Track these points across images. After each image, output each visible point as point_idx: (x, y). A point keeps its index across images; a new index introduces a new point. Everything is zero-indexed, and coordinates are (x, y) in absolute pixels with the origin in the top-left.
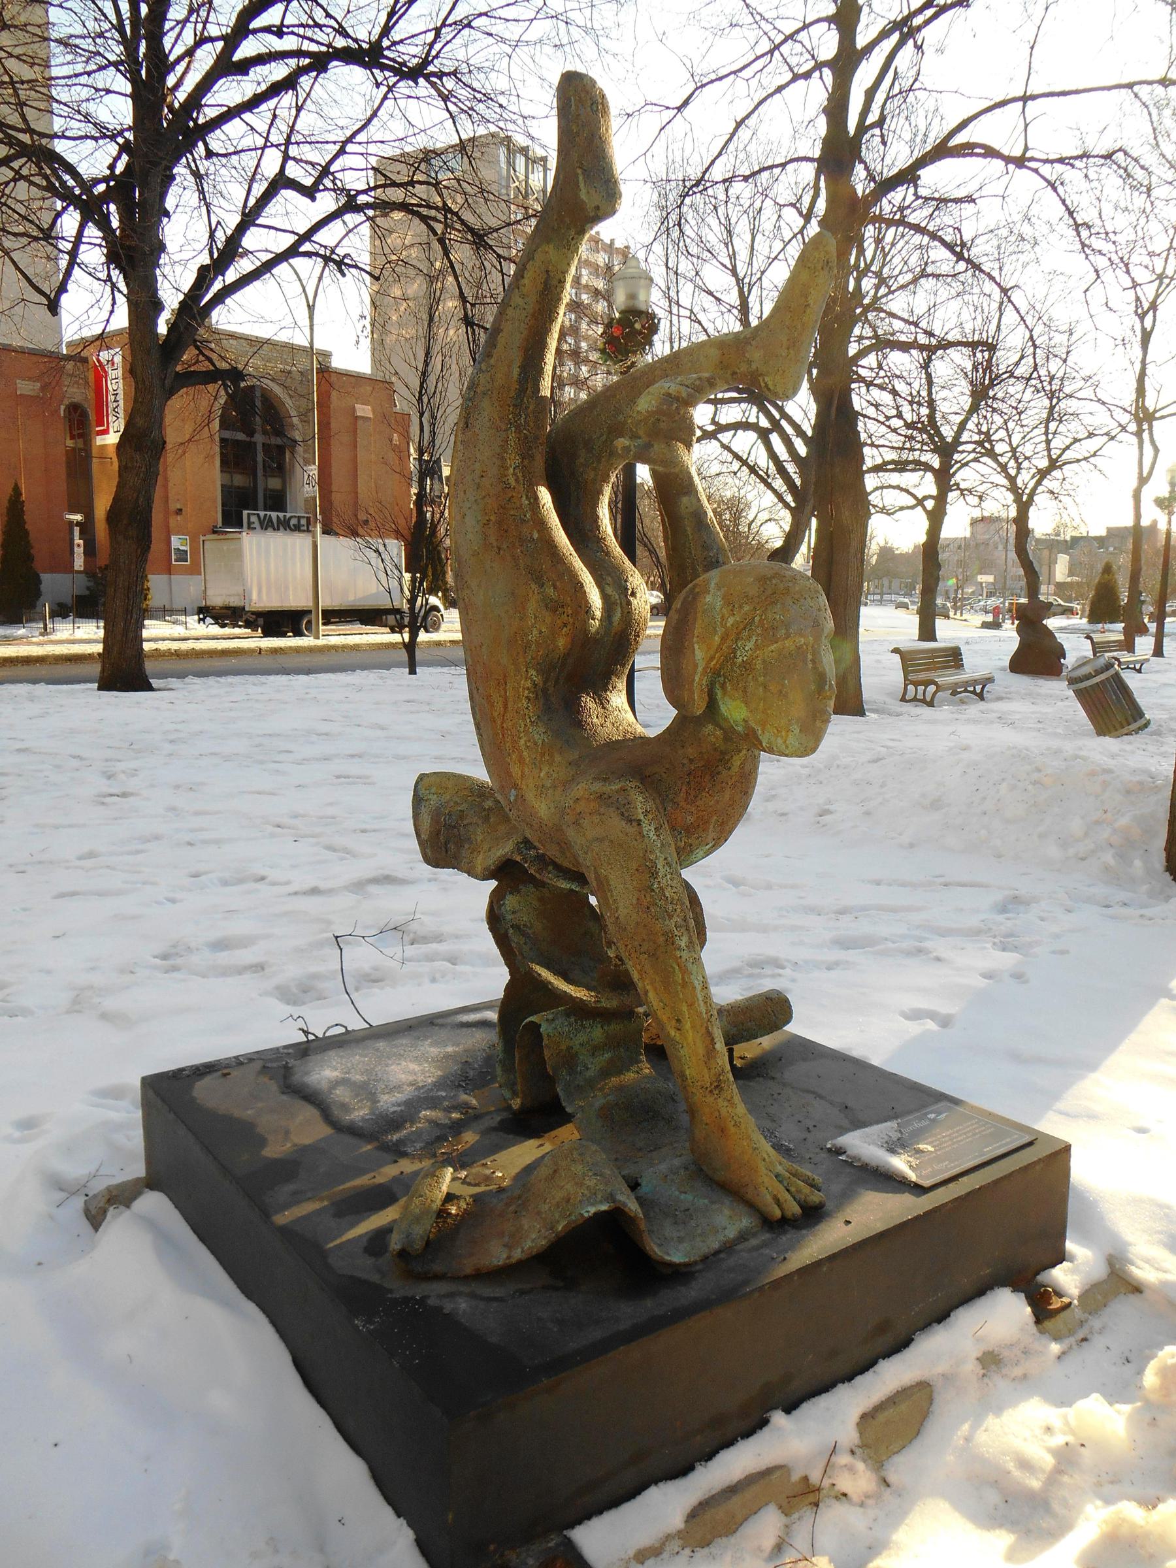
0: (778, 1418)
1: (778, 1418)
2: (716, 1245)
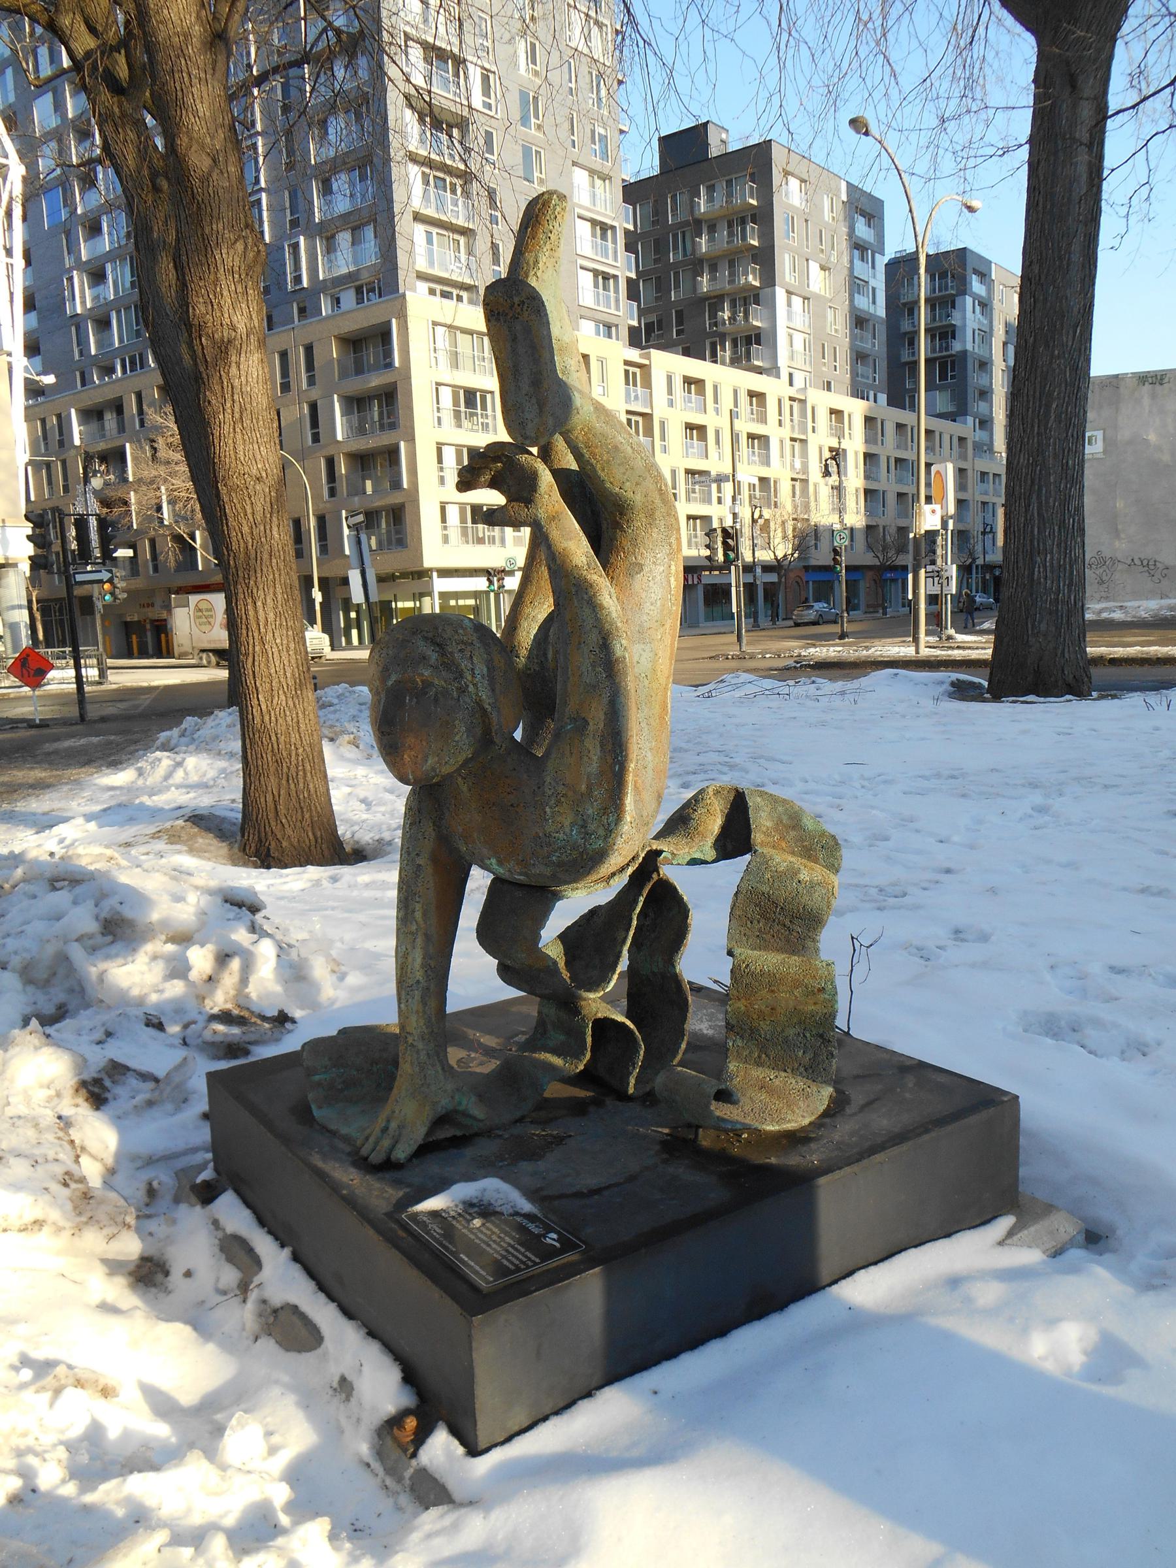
0: (286, 1252)
1: (286, 1252)
2: (333, 1127)
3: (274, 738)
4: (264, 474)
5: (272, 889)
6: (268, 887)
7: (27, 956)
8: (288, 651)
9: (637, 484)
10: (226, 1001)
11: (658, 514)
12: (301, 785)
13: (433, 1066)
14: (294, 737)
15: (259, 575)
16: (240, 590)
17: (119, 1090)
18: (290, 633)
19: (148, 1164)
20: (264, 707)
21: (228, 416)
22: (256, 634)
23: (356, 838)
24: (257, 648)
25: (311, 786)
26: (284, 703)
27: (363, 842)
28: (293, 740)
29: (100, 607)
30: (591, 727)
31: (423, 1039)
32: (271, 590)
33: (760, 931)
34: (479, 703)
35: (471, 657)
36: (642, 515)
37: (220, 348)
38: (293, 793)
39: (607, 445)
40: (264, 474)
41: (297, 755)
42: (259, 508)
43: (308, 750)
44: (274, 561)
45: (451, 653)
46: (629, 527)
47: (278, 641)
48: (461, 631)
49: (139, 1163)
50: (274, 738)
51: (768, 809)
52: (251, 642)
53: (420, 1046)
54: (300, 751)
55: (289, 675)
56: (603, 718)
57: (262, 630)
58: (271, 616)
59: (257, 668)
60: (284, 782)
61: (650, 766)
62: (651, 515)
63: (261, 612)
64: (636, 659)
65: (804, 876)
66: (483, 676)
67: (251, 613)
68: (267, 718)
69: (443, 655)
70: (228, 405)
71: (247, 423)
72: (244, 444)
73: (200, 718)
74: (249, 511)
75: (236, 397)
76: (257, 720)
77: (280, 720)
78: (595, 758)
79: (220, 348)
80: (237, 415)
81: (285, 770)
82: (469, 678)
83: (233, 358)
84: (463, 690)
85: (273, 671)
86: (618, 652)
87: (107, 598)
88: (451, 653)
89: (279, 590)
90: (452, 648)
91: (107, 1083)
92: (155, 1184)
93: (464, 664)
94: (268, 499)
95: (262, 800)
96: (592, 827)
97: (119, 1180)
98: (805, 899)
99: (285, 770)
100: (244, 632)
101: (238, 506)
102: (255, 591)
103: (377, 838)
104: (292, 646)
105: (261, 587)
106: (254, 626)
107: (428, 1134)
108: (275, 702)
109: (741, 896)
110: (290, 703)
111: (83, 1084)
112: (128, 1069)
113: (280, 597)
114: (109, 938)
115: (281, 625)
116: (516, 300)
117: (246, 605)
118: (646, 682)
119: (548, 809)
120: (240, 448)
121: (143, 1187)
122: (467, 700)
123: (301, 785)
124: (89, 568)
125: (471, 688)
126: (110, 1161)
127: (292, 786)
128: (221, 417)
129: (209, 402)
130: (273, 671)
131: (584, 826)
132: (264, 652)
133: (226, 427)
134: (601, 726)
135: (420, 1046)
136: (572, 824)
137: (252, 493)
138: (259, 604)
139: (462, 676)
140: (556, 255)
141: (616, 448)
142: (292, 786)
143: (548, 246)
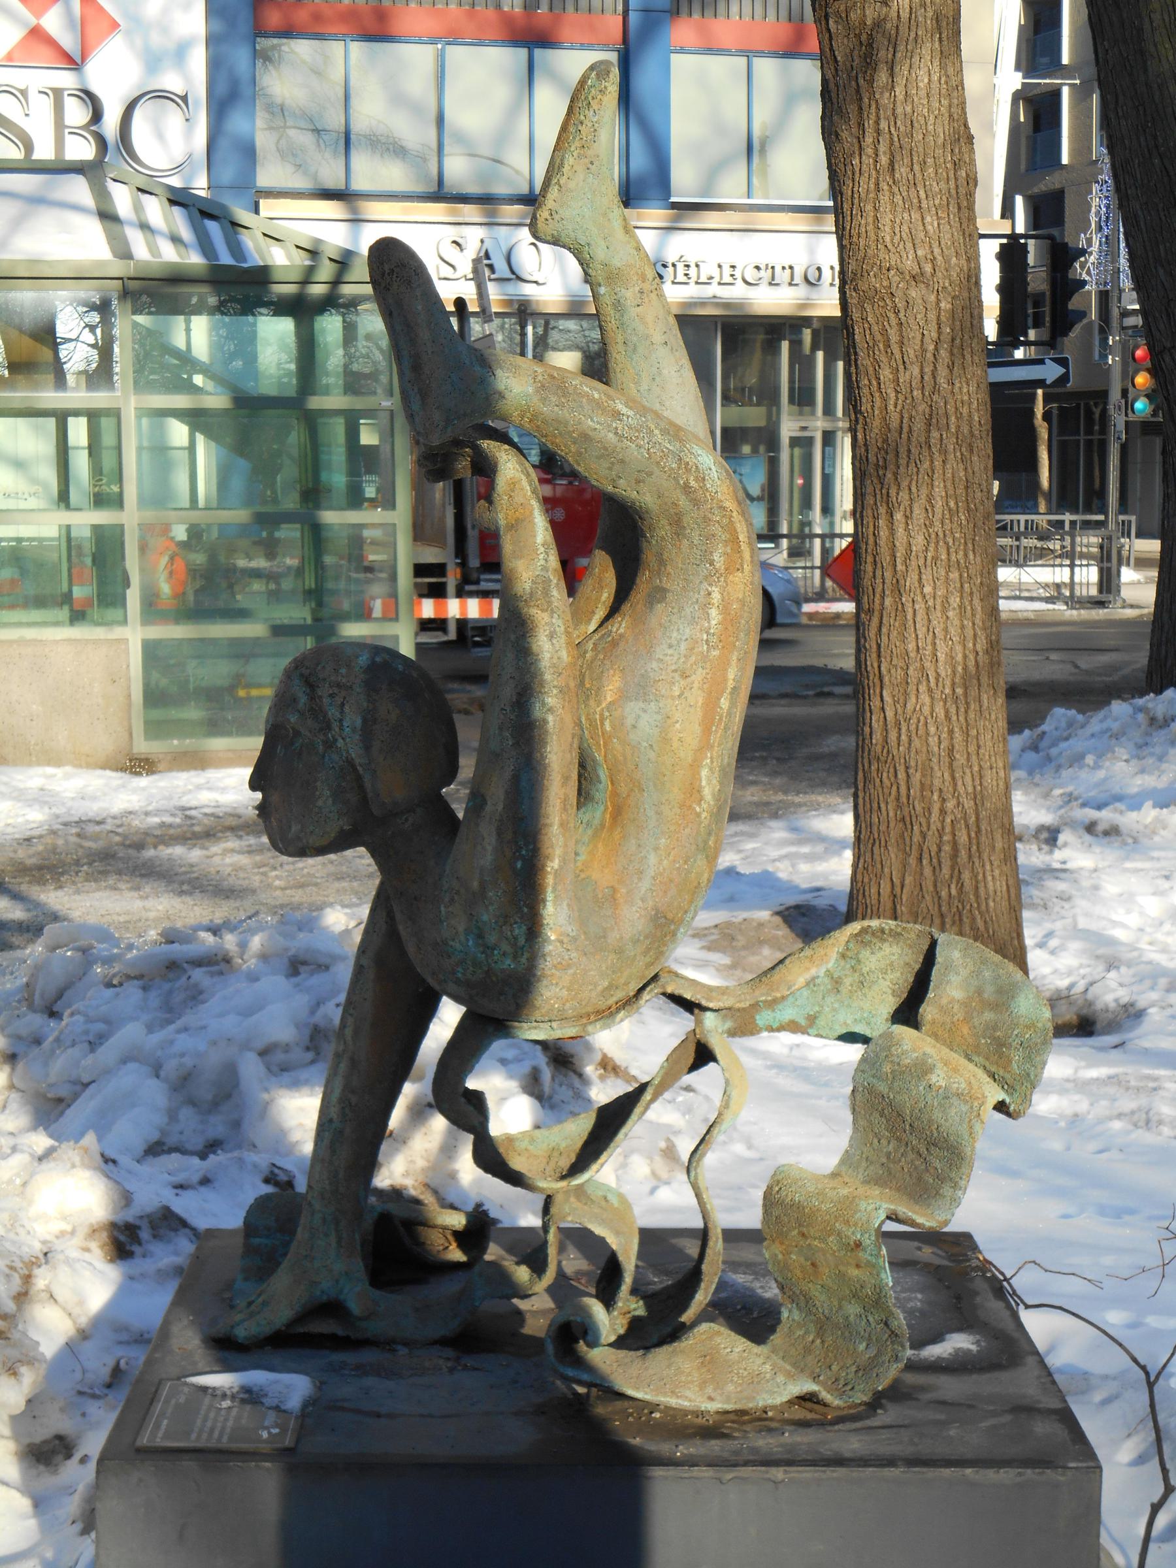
3: (901, 775)
4: (928, 268)
5: (795, 1052)
6: (791, 1049)
7: (188, 1062)
8: (944, 610)
9: (638, 482)
10: (406, 1174)
11: (686, 520)
12: (946, 871)
13: (326, 1235)
14: (940, 776)
15: (903, 462)
16: (870, 489)
17: (157, 1248)
18: (954, 575)
19: (136, 1341)
20: (890, 714)
21: (868, 161)
22: (888, 575)
23: (1090, 996)
24: (888, 601)
25: (966, 876)
26: (926, 710)
27: (1099, 1006)
28: (937, 783)
29: (1121, 426)
30: (489, 808)
31: (323, 1199)
32: (924, 491)
33: (888, 1155)
34: (350, 762)
35: (343, 705)
36: (664, 522)
37: (858, 36)
38: (928, 885)
39: (570, 433)
40: (928, 268)
41: (943, 812)
42: (914, 334)
43: (968, 804)
44: (935, 434)
45: (320, 697)
46: (652, 537)
47: (928, 589)
48: (343, 671)
49: (124, 1337)
50: (901, 775)
51: (964, 973)
52: (879, 590)
53: (317, 1205)
54: (950, 805)
55: (941, 656)
56: (502, 797)
57: (900, 567)
58: (919, 541)
59: (884, 638)
60: (912, 861)
61: (651, 872)
62: (677, 522)
63: (900, 531)
64: (629, 721)
65: (938, 1078)
66: (354, 730)
67: (884, 533)
68: (893, 735)
69: (312, 699)
70: (869, 140)
71: (902, 171)
72: (894, 211)
73: (1080, 711)
74: (894, 338)
75: (884, 125)
76: (877, 737)
77: (916, 743)
78: (489, 848)
79: (858, 36)
80: (884, 160)
81: (917, 838)
82: (337, 730)
83: (882, 53)
84: (330, 745)
85: (911, 646)
86: (537, 712)
87: (1139, 405)
88: (320, 697)
89: (939, 491)
90: (323, 691)
91: (145, 1235)
92: (122, 1363)
93: (333, 713)
94: (932, 316)
95: (874, 890)
96: (492, 939)
97: (88, 1347)
98: (937, 1115)
99: (917, 838)
100: (869, 568)
101: (875, 328)
102: (893, 492)
103: (1125, 1000)
104: (955, 601)
105: (904, 484)
106: (886, 559)
107: (301, 1318)
108: (910, 706)
109: (859, 1097)
110: (940, 711)
111: (113, 1226)
112: (184, 1223)
113: (939, 504)
114: (310, 1055)
115: (935, 559)
116: (387, 268)
117: (876, 518)
118: (652, 755)
119: (442, 909)
120: (886, 220)
121: (111, 1363)
122: (335, 757)
123: (946, 871)
124: (1019, 354)
125: (340, 743)
126: (83, 1321)
127: (927, 871)
128: (856, 162)
129: (837, 135)
130: (911, 646)
131: (480, 936)
132: (900, 609)
133: (863, 180)
134: (500, 807)
135: (317, 1205)
136: (468, 931)
137: (901, 305)
138: (899, 516)
139: (329, 727)
140: (590, 153)
141: (585, 437)
142: (927, 871)
143: (577, 144)
